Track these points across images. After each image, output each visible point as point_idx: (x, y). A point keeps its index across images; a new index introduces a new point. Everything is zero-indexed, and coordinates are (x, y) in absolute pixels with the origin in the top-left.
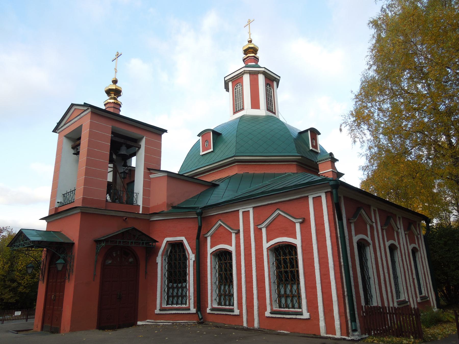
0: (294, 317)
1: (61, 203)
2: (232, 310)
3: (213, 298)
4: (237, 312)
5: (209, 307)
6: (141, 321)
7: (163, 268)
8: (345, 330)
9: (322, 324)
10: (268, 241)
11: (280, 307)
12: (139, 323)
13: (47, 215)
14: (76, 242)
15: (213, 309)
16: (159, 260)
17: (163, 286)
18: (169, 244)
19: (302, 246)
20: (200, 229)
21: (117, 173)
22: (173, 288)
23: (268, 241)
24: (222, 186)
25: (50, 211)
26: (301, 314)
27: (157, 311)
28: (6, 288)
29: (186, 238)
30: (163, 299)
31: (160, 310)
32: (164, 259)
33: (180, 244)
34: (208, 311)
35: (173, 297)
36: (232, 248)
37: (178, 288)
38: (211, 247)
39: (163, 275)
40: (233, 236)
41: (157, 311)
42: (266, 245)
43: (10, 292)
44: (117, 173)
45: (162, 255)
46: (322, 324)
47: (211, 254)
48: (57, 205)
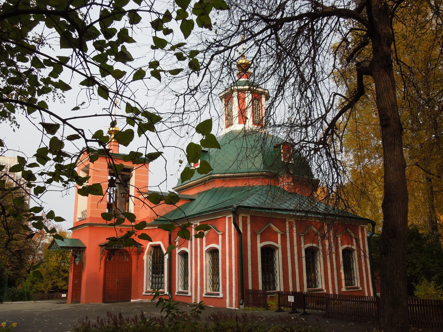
0: (216, 296)
1: (80, 218)
2: (187, 293)
3: (180, 285)
4: (190, 294)
5: (177, 291)
6: (133, 299)
7: (148, 264)
8: (239, 305)
9: (228, 301)
10: (261, 242)
11: (213, 291)
12: (132, 301)
13: (72, 226)
14: (87, 246)
15: (179, 292)
16: (145, 258)
17: (148, 276)
18: (152, 246)
19: (222, 250)
20: (170, 236)
21: (393, 43)
22: (156, 278)
23: (261, 242)
24: (198, 200)
25: (74, 223)
26: (218, 295)
27: (144, 293)
28: (59, 277)
29: (162, 242)
30: (148, 285)
31: (146, 292)
32: (148, 257)
33: (159, 247)
34: (176, 294)
35: (155, 284)
36: (219, 247)
37: (159, 278)
38: (206, 246)
39: (148, 268)
40: (220, 237)
41: (144, 293)
42: (205, 249)
43: (63, 281)
44: (393, 43)
45: (147, 254)
46: (228, 301)
47: (178, 254)
48: (78, 220)
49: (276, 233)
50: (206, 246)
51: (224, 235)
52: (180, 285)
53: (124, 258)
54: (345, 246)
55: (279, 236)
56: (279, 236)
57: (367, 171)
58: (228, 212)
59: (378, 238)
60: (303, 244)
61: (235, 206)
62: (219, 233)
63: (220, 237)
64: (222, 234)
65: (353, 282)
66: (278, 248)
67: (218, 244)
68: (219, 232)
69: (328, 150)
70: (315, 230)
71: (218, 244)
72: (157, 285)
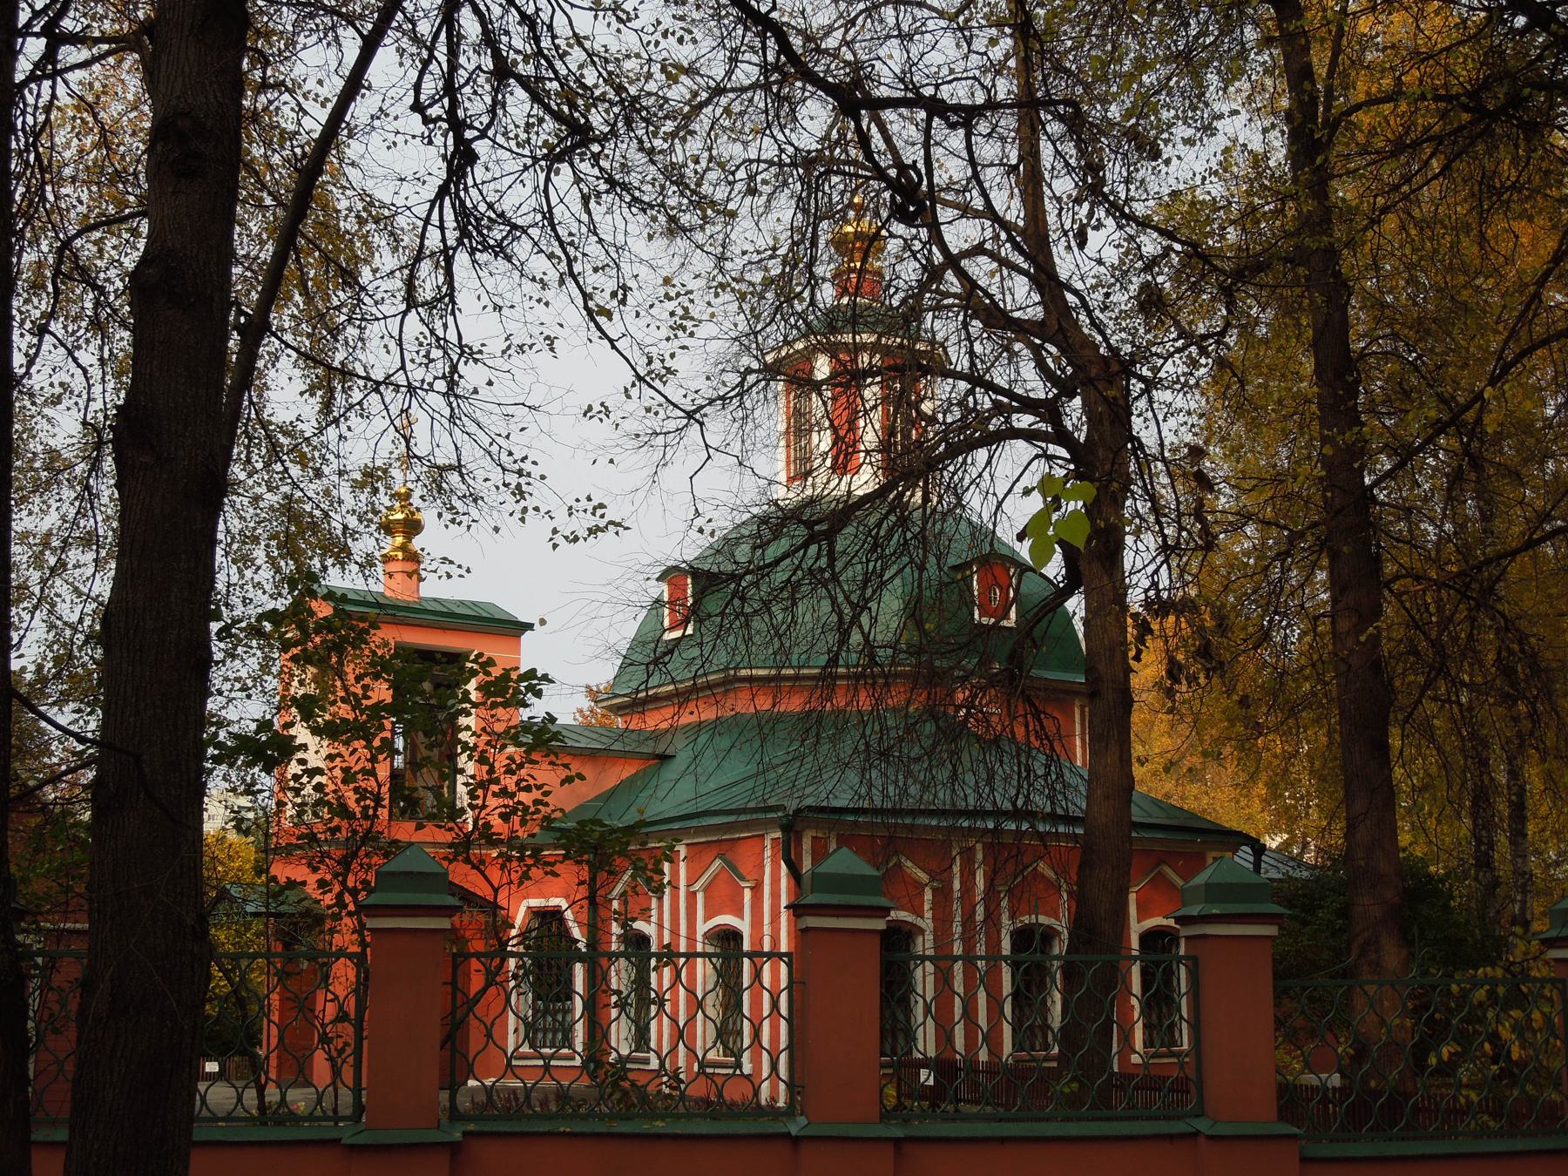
3: (623, 1036)
37: (556, 1012)
38: (707, 918)
40: (747, 894)
42: (702, 928)
49: (920, 887)
50: (707, 918)
51: (757, 889)
52: (623, 1036)
53: (1065, 738)
54: (1157, 921)
55: (928, 895)
56: (928, 895)
57: (991, 758)
58: (768, 825)
59: (1280, 880)
60: (1005, 920)
61: (792, 805)
62: (743, 884)
63: (747, 894)
64: (752, 888)
65: (1177, 1034)
66: (922, 931)
67: (740, 915)
68: (743, 879)
69: (234, 341)
70: (1050, 874)
71: (740, 915)
72: (550, 1036)
